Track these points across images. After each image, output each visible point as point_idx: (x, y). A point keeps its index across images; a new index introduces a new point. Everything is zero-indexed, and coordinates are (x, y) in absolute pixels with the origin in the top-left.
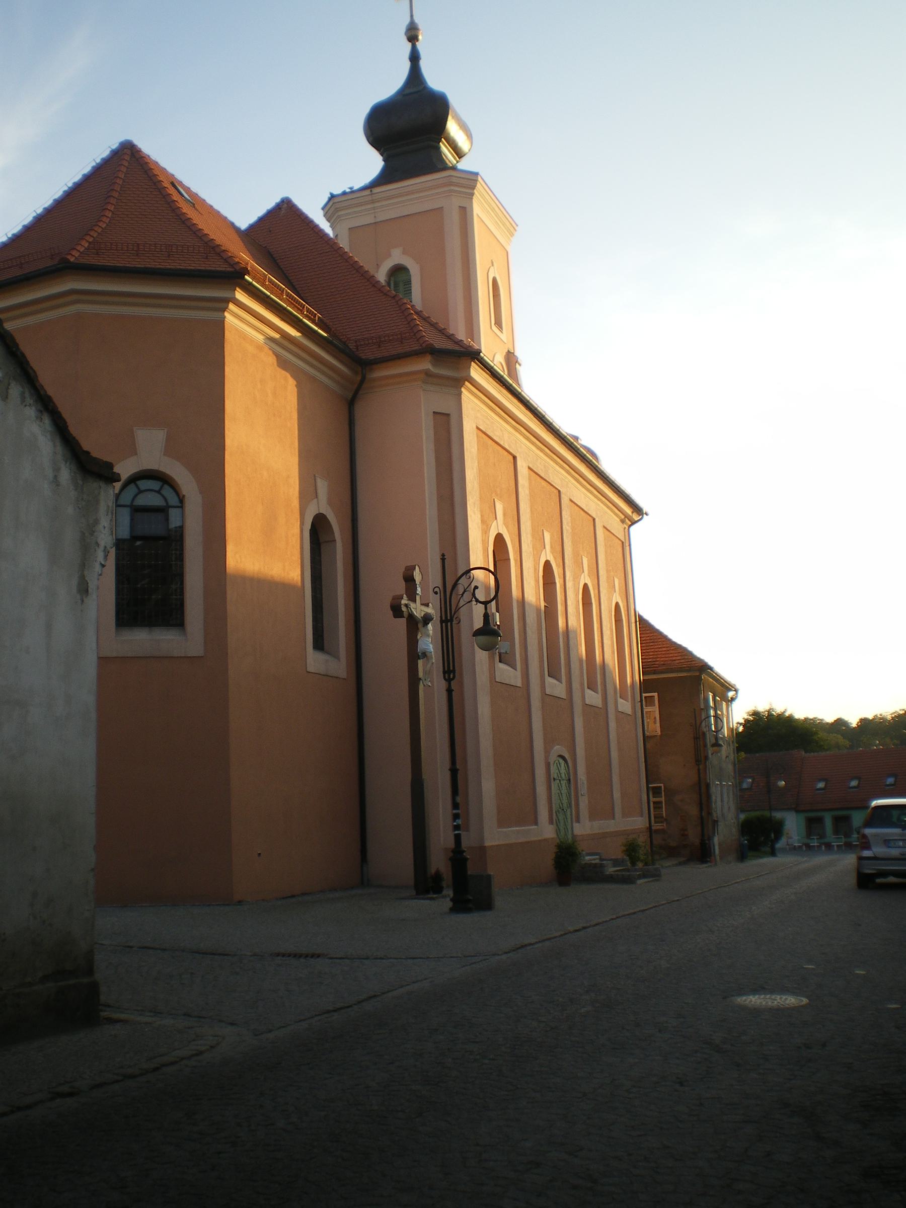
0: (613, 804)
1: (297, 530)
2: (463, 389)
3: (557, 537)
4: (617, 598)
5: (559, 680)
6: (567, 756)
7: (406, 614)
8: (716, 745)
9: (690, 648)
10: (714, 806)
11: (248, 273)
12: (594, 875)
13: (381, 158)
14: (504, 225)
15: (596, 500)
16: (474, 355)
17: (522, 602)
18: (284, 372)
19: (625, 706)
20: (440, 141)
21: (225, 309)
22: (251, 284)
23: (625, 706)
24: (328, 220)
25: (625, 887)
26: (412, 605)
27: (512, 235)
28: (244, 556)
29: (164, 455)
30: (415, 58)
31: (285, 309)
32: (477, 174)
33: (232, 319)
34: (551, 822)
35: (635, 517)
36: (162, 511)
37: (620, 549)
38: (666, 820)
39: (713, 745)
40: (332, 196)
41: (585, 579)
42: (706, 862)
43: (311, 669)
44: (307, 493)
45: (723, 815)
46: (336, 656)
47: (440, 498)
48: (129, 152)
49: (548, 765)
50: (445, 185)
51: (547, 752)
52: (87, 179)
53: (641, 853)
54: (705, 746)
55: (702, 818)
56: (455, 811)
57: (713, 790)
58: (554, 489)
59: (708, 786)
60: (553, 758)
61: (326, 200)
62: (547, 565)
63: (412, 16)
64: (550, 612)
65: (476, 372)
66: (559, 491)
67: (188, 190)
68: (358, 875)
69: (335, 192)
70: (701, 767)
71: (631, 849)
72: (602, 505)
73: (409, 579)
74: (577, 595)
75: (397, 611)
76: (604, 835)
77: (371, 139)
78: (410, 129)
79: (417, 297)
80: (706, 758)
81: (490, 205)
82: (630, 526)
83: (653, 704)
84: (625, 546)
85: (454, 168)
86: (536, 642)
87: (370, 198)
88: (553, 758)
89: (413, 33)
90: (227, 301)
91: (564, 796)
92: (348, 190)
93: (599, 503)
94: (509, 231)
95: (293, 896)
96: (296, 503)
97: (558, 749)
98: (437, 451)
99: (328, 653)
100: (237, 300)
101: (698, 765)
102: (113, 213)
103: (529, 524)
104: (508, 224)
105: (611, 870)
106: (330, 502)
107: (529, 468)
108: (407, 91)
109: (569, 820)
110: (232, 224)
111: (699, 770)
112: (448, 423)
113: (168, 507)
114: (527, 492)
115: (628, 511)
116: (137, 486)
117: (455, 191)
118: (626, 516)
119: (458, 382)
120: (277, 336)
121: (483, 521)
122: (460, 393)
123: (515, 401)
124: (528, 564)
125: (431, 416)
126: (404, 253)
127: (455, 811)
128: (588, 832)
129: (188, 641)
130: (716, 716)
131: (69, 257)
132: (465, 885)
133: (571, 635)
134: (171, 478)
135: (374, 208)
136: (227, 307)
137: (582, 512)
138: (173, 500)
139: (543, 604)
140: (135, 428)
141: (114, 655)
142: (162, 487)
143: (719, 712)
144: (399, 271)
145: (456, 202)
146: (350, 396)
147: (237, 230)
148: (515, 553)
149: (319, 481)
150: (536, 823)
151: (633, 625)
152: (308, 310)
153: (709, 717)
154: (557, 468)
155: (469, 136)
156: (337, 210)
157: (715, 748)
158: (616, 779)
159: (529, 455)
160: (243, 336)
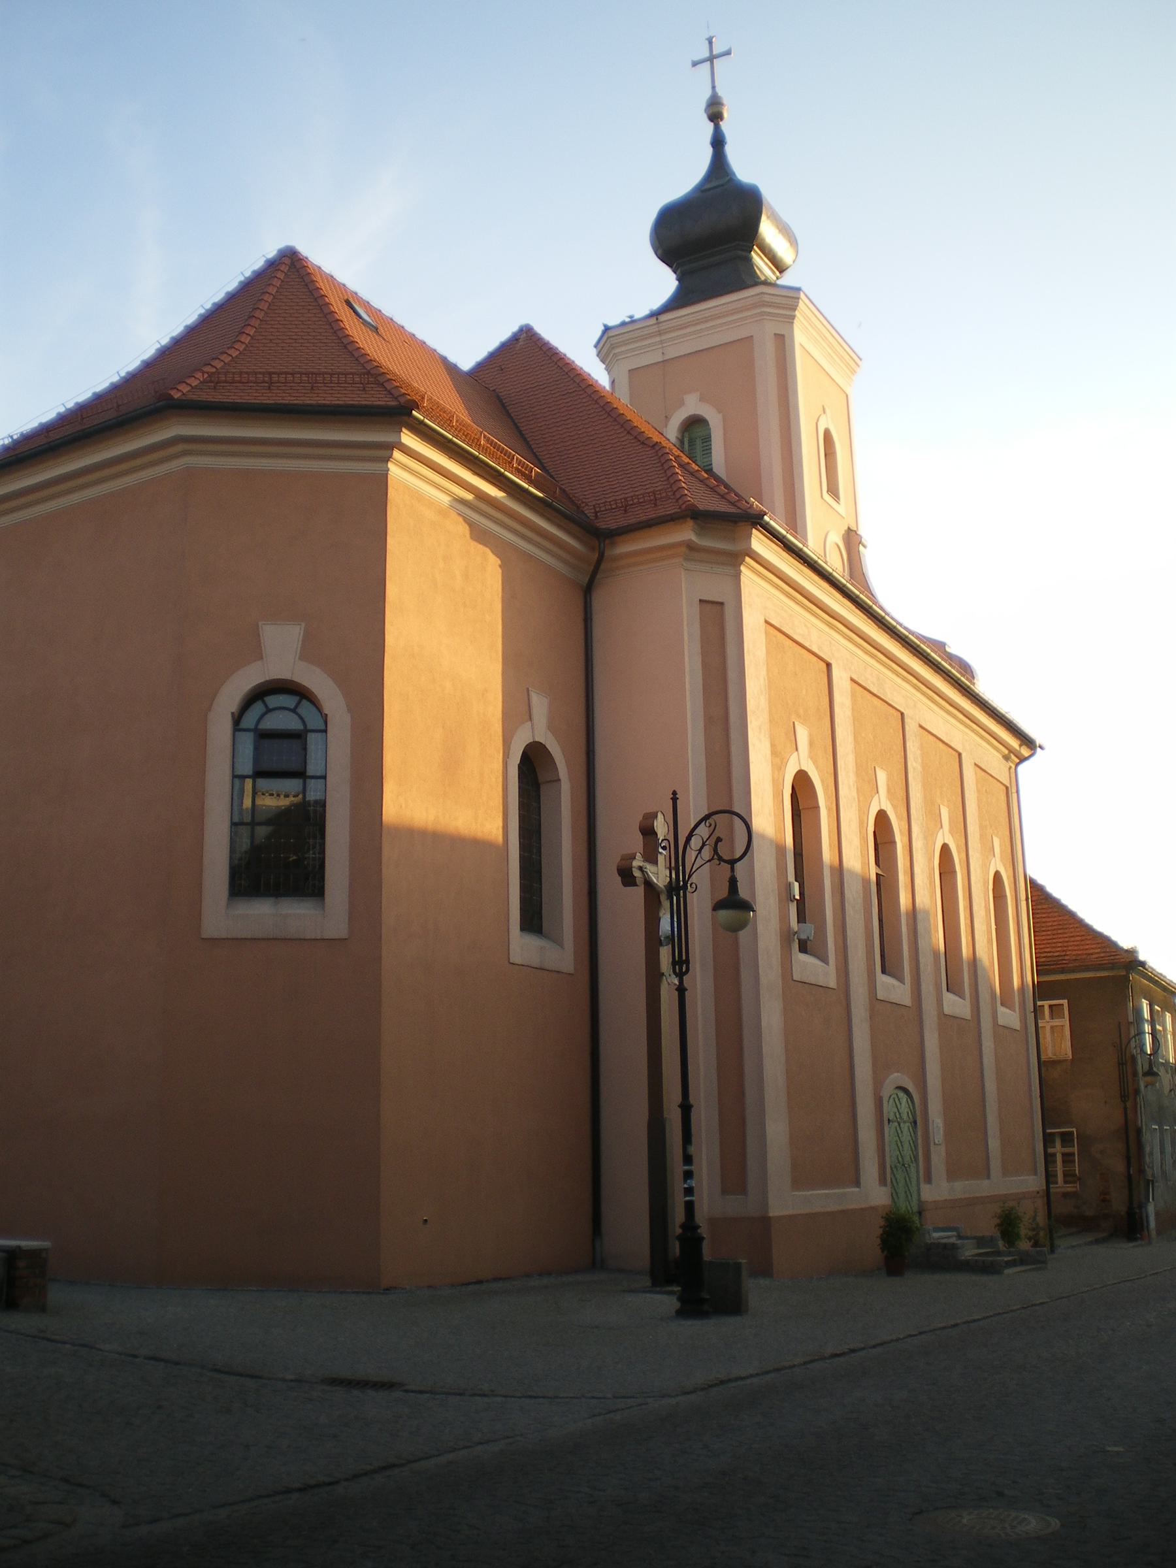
0: (988, 1158)
2: (742, 568)
3: (899, 778)
4: (997, 864)
5: (901, 979)
6: (911, 1088)
7: (639, 881)
8: (1150, 1073)
9: (1114, 938)
10: (1147, 1160)
11: (417, 407)
12: (942, 1260)
13: (674, 276)
14: (841, 358)
16: (756, 520)
17: (839, 870)
18: (480, 546)
19: (1010, 1017)
20: (751, 249)
21: (388, 459)
22: (422, 422)
23: (1010, 1017)
24: (603, 361)
25: (985, 1278)
26: (650, 868)
27: (854, 372)
28: (407, 800)
30: (718, 142)
31: (477, 458)
32: (798, 290)
33: (399, 471)
34: (883, 1181)
35: (1025, 752)
36: (298, 737)
37: (1003, 797)
38: (1079, 1179)
39: (1145, 1074)
40: (607, 329)
41: (945, 836)
42: (1135, 1239)
43: (516, 958)
45: (1164, 1173)
46: (558, 942)
47: (709, 720)
48: (288, 261)
49: (879, 1102)
50: (755, 306)
51: (878, 1084)
52: (232, 299)
54: (1135, 1074)
55: (1129, 1178)
56: (686, 1168)
57: (1146, 1137)
58: (893, 711)
59: (1139, 1131)
60: (888, 1090)
61: (599, 333)
63: (714, 87)
64: (885, 885)
65: (759, 543)
66: (902, 714)
67: (367, 305)
68: (587, 1255)
69: (611, 324)
70: (1129, 1104)
71: (1008, 1225)
73: (648, 832)
74: (931, 860)
75: (627, 876)
76: (971, 1202)
77: (660, 252)
78: (712, 236)
79: (718, 460)
80: (1137, 1092)
82: (1017, 765)
84: (1010, 792)
85: (774, 285)
87: (655, 328)
88: (888, 1090)
89: (715, 110)
90: (391, 447)
91: (906, 1145)
92: (628, 320)
95: (480, 1282)
96: (497, 727)
97: (896, 1078)
98: (705, 654)
99: (547, 937)
100: (404, 445)
101: (1124, 1102)
103: (851, 759)
104: (847, 357)
105: (969, 1252)
106: (551, 727)
107: (852, 680)
108: (708, 186)
110: (444, 360)
111: (1125, 1108)
112: (722, 615)
113: (307, 731)
114: (849, 713)
115: (1014, 743)
119: (736, 558)
120: (469, 497)
121: (774, 753)
122: (737, 576)
124: (849, 816)
125: (696, 607)
126: (702, 399)
127: (686, 1168)
130: (1154, 1033)
131: (172, 393)
132: (696, 1274)
133: (919, 917)
134: (259, 686)
135: (661, 342)
136: (391, 456)
137: (941, 744)
138: (314, 722)
139: (873, 870)
140: (260, 624)
141: (224, 935)
143: (1159, 1027)
144: (695, 426)
145: (771, 328)
147: (451, 369)
148: (827, 799)
149: (535, 698)
150: (857, 1183)
151: (1024, 904)
152: (519, 463)
153: (1141, 1033)
154: (899, 681)
156: (613, 347)
157: (1149, 1079)
159: (850, 662)
160: (419, 497)
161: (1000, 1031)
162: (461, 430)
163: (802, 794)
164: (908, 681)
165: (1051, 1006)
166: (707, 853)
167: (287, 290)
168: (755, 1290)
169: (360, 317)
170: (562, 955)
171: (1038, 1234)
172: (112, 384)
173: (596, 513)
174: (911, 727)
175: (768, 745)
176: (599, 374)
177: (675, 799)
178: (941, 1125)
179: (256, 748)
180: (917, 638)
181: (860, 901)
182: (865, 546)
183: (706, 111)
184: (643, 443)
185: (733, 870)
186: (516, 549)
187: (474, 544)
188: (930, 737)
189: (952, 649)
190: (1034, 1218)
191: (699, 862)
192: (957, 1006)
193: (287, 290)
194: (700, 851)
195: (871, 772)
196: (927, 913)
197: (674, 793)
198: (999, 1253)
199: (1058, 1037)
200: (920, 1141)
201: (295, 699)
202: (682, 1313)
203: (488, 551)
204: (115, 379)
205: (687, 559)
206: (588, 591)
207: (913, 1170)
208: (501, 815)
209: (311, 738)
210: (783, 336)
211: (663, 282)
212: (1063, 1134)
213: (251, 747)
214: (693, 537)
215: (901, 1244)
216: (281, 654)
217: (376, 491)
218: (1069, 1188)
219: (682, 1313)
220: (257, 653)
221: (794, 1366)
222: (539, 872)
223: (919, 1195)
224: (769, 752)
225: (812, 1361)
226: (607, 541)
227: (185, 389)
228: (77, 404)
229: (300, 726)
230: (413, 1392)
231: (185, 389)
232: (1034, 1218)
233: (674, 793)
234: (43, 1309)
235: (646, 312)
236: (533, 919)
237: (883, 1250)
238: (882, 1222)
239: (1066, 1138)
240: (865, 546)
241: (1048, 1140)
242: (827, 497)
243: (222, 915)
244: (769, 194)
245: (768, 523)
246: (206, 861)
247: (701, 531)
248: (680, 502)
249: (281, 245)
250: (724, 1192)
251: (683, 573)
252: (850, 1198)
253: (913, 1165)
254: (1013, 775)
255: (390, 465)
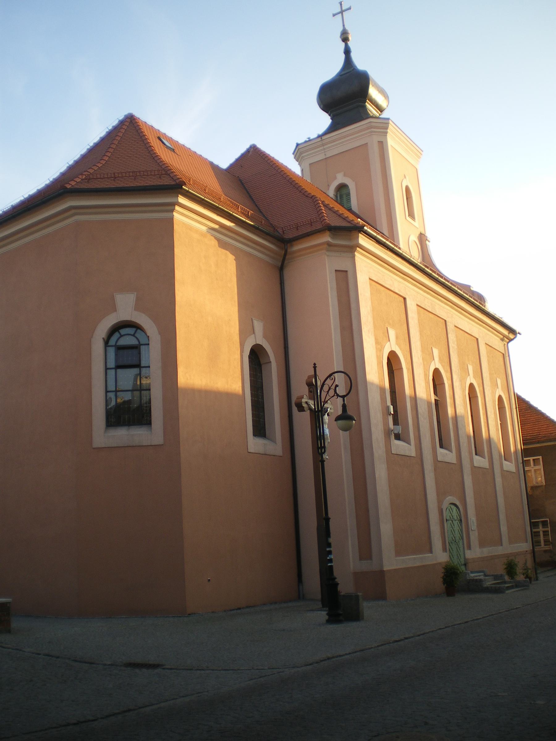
1: (238, 356)
2: (356, 253)
4: (500, 392)
5: (451, 451)
6: (458, 503)
11: (185, 184)
13: (329, 117)
15: (478, 326)
17: (415, 399)
18: (224, 251)
19: (510, 466)
21: (173, 210)
23: (510, 466)
24: (297, 160)
27: (419, 157)
29: (135, 310)
30: (347, 52)
31: (218, 207)
32: (388, 119)
33: (179, 216)
34: (445, 550)
35: (511, 336)
36: (136, 348)
37: (502, 359)
38: (552, 543)
40: (298, 145)
41: (471, 379)
44: (245, 330)
46: (274, 441)
47: (342, 329)
48: (129, 120)
49: (441, 512)
51: (440, 502)
53: (519, 570)
58: (441, 320)
60: (445, 505)
62: (437, 372)
63: (344, 26)
64: (439, 405)
65: (363, 240)
66: (445, 321)
67: (170, 140)
69: (299, 142)
71: (510, 568)
72: (484, 329)
74: (464, 391)
76: (493, 558)
77: (322, 106)
78: (347, 97)
79: (354, 204)
81: (400, 139)
82: (508, 343)
83: (539, 464)
84: (505, 356)
85: (378, 118)
86: (428, 426)
88: (445, 505)
91: (457, 532)
92: (307, 140)
93: (481, 327)
94: (416, 155)
95: (239, 609)
96: (236, 338)
97: (450, 499)
102: (109, 158)
104: (415, 151)
106: (265, 337)
107: (417, 305)
108: (343, 73)
109: (461, 549)
110: (212, 164)
112: (347, 277)
114: (416, 321)
115: (505, 332)
116: (119, 332)
117: (375, 132)
118: (504, 336)
119: (352, 248)
120: (217, 227)
121: (377, 342)
122: (354, 257)
123: (400, 260)
125: (334, 273)
126: (345, 175)
128: (479, 555)
129: (152, 435)
133: (459, 419)
135: (324, 149)
136: (174, 209)
137: (467, 335)
139: (433, 398)
141: (103, 446)
142: (136, 332)
144: (342, 188)
145: (376, 139)
146: (279, 264)
147: (215, 168)
149: (256, 323)
151: (515, 410)
155: (386, 96)
156: (301, 153)
158: (502, 517)
159: (415, 296)
160: (190, 228)
161: (505, 474)
162: (211, 194)
163: (393, 363)
164: (448, 305)
165: (534, 460)
166: (332, 392)
167: (129, 134)
168: (368, 608)
169: (165, 145)
170: (275, 447)
171: (528, 571)
172: (46, 185)
173: (283, 231)
174: (450, 327)
175: (374, 339)
176: (295, 168)
177: (315, 367)
178: (475, 521)
179: (116, 355)
180: (451, 284)
181: (427, 413)
182: (429, 241)
183: (340, 37)
184: (307, 196)
185: (344, 400)
186: (242, 250)
187: (220, 249)
188: (461, 331)
189: (474, 288)
190: (525, 564)
191: (328, 398)
192: (480, 462)
193: (129, 134)
194: (328, 392)
195: (430, 350)
196: (463, 417)
197: (315, 364)
198: (505, 582)
199: (537, 475)
200: (464, 529)
201: (134, 329)
202: (329, 621)
203: (228, 253)
204: (48, 182)
205: (328, 251)
206: (281, 269)
207: (461, 544)
208: (240, 381)
209: (143, 348)
210: (382, 142)
211: (324, 120)
212: (543, 522)
213: (114, 354)
214: (330, 239)
215: (453, 580)
216: (125, 308)
217: (168, 226)
218: (547, 548)
219: (329, 621)
220: (114, 309)
221: (372, 648)
222: (263, 408)
223: (465, 557)
224: (374, 344)
225: (382, 645)
226: (288, 245)
227: (73, 183)
228: (29, 195)
229: (137, 343)
230: (167, 669)
231: (73, 183)
232: (525, 564)
233: (315, 364)
234: (9, 631)
235: (316, 136)
236: (260, 429)
237: (444, 584)
238: (443, 570)
239: (544, 524)
240: (429, 241)
241: (533, 525)
242: (408, 218)
243: (102, 436)
244: (372, 74)
245: (366, 230)
246: (93, 410)
247: (334, 237)
248: (323, 223)
249: (126, 113)
250: (361, 559)
251: (326, 257)
252: (427, 559)
253: (461, 541)
254: (506, 348)
255: (175, 214)
